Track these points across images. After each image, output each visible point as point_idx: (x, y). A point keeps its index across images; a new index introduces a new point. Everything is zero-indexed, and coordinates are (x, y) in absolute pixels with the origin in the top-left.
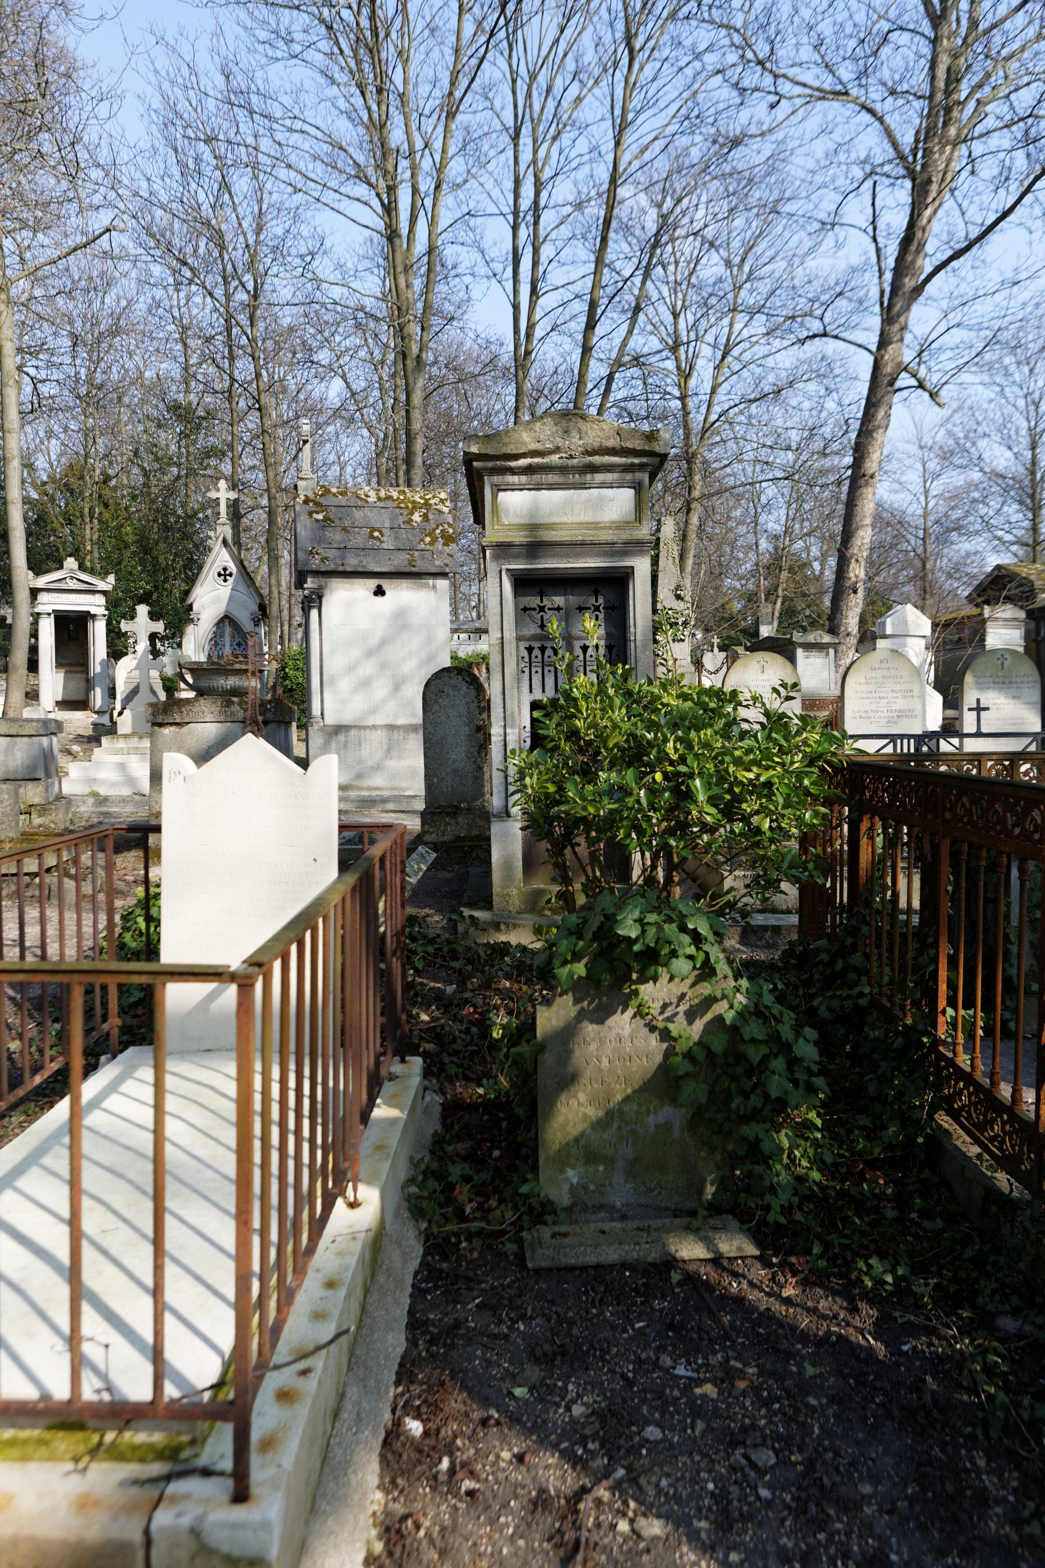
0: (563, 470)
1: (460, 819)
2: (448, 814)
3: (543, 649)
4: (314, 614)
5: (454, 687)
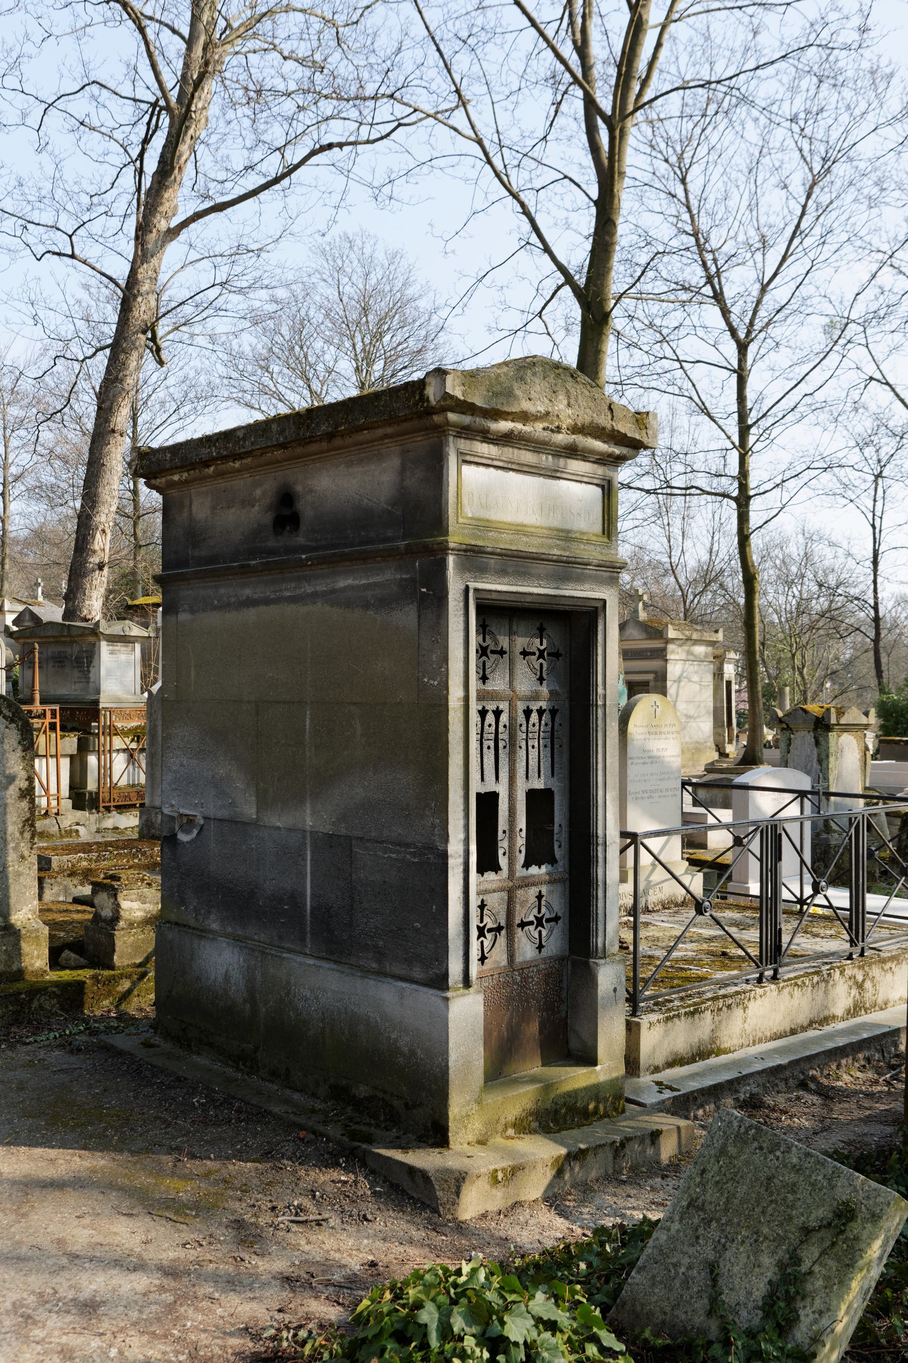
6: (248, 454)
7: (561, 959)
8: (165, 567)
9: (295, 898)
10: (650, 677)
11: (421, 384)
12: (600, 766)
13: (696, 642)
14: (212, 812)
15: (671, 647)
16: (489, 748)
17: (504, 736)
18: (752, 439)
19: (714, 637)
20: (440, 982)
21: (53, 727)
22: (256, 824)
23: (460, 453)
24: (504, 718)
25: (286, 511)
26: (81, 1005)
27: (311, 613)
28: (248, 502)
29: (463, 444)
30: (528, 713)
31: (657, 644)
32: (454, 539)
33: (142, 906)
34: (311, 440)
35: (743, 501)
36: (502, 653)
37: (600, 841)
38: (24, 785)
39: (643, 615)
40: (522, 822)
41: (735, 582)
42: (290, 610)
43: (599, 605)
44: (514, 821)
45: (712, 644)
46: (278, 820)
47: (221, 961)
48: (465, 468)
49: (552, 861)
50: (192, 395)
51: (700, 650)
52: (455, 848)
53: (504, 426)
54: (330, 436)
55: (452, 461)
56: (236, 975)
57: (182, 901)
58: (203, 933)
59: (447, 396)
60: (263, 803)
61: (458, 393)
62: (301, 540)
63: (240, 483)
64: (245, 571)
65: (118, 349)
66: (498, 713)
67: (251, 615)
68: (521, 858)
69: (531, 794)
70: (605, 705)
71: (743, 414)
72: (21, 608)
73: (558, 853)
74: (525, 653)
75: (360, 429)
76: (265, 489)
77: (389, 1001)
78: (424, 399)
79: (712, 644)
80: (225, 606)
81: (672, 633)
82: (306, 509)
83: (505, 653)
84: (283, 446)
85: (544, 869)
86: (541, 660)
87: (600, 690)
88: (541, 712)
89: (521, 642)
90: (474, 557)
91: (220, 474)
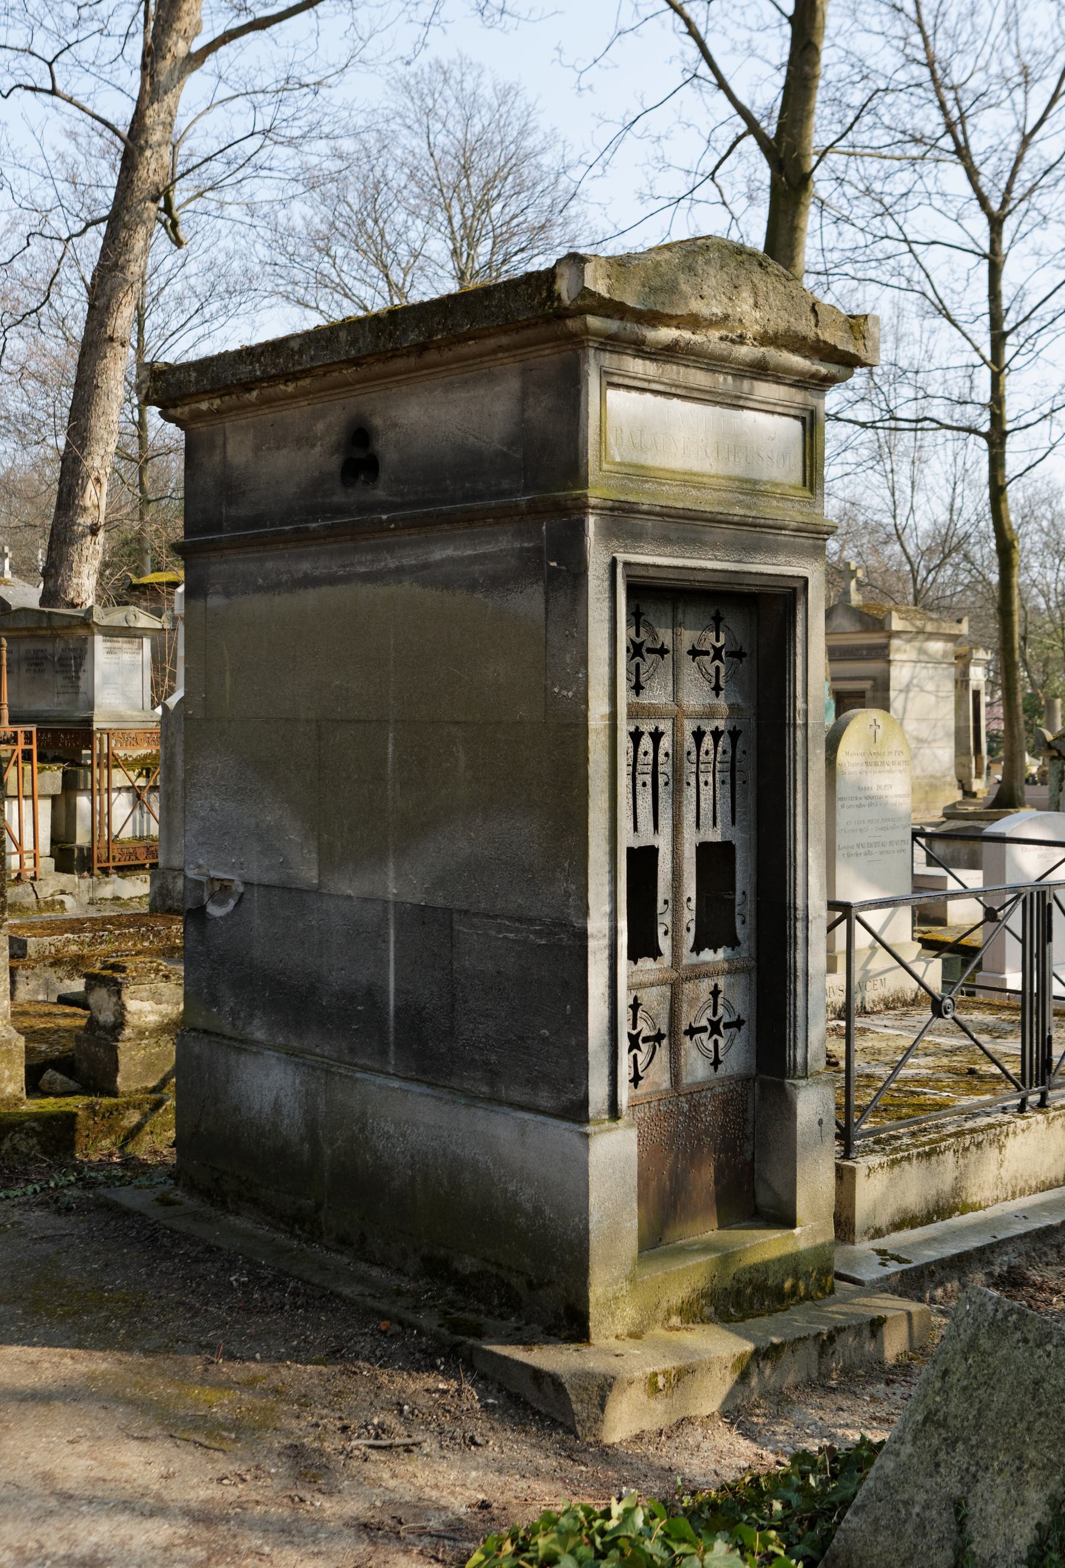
6: (306, 373)
7: (745, 1080)
9: (373, 996)
10: (867, 685)
11: (549, 276)
12: (800, 810)
15: (895, 643)
16: (706, 783)
17: (665, 767)
18: (1008, 352)
20: (577, 1111)
21: (27, 756)
22: (317, 892)
23: (604, 373)
24: (666, 744)
25: (359, 453)
26: (71, 1146)
28: (306, 441)
29: (609, 360)
30: (698, 735)
31: (876, 639)
32: (595, 495)
34: (395, 354)
36: (662, 651)
37: (800, 914)
40: (690, 889)
41: (986, 551)
42: (365, 591)
43: (798, 584)
44: (679, 885)
45: (954, 638)
46: (348, 886)
47: (269, 1085)
48: (612, 394)
49: (733, 942)
50: (221, 288)
51: (937, 647)
52: (597, 924)
53: (666, 334)
54: (422, 348)
57: (215, 1000)
58: (242, 1044)
59: (585, 293)
60: (328, 862)
62: (380, 494)
63: (295, 415)
64: (302, 537)
65: (119, 223)
66: (656, 736)
67: (310, 598)
68: (689, 939)
69: (704, 850)
70: (806, 725)
71: (996, 317)
74: (694, 653)
75: (464, 338)
77: (503, 1138)
78: (553, 296)
79: (954, 638)
80: (274, 587)
81: (897, 624)
82: (388, 451)
83: (667, 651)
84: (355, 362)
85: (721, 954)
86: (717, 662)
87: (800, 704)
88: (716, 734)
89: (688, 637)
90: (622, 517)
91: (266, 402)
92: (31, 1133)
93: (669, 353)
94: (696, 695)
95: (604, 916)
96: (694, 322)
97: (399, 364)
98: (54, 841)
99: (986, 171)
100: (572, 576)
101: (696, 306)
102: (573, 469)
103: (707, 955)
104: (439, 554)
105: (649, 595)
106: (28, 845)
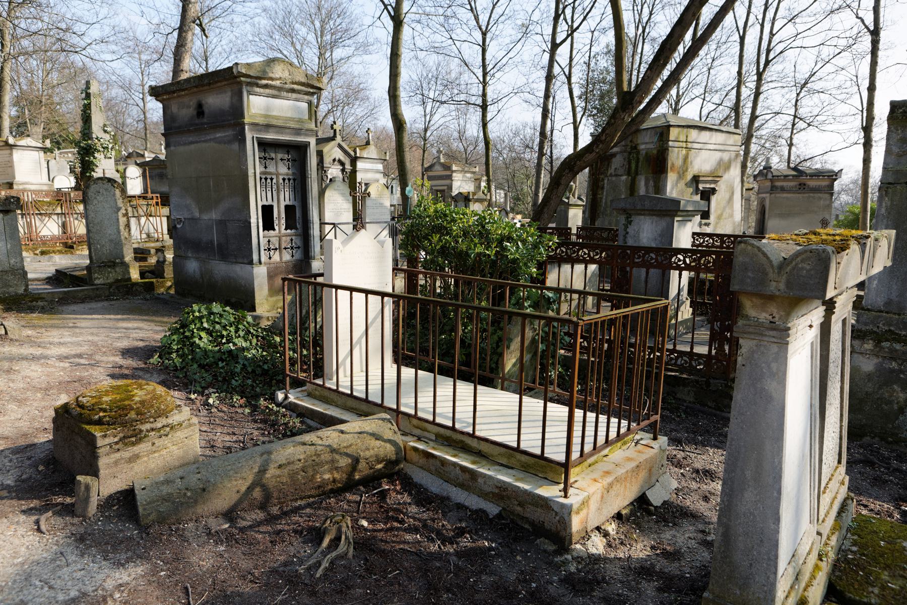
0: (280, 89)
1: (117, 269)
2: (109, 267)
3: (266, 179)
4: (701, 179)
5: (106, 190)
6: (186, 89)
7: (301, 261)
8: (165, 129)
9: (212, 242)
10: (445, 188)
11: (230, 68)
13: (466, 172)
14: (186, 217)
15: (454, 174)
17: (275, 187)
18: (488, 78)
19: (474, 170)
20: (251, 263)
21: (157, 204)
22: (199, 219)
23: (248, 91)
24: (274, 181)
25: (200, 110)
26: (153, 290)
27: (208, 146)
28: (189, 107)
29: (249, 88)
30: (284, 180)
31: (448, 173)
32: (246, 120)
33: (399, 439)
34: (203, 86)
35: (484, 107)
36: (272, 159)
38: (124, 212)
39: (442, 161)
40: (283, 215)
41: (482, 145)
42: (204, 145)
44: (279, 215)
45: (474, 173)
46: (205, 217)
47: (192, 266)
48: (251, 97)
49: (296, 229)
50: (234, 50)
51: (469, 175)
52: (253, 220)
53: (264, 82)
54: (210, 84)
55: (245, 94)
56: (197, 270)
57: (180, 248)
58: (186, 258)
59: (239, 72)
60: (201, 212)
61: (244, 71)
62: (205, 120)
63: (186, 100)
64: (189, 131)
65: (182, 30)
66: (272, 179)
67: (193, 147)
68: (284, 227)
69: (287, 207)
71: (484, 66)
72: (153, 156)
73: (298, 226)
74: (282, 160)
75: (216, 82)
76: (193, 102)
77: (238, 270)
78: (233, 73)
79: (474, 173)
80: (185, 144)
81: (454, 168)
82: (206, 111)
84: (196, 87)
85: (293, 231)
88: (289, 180)
89: (280, 156)
90: (254, 125)
91: (179, 96)
92: (141, 286)
93: (266, 86)
94: (283, 169)
95: (255, 218)
96: (272, 79)
97: (205, 88)
98: (168, 230)
99: (481, 18)
100: (243, 141)
101: (271, 75)
102: (242, 115)
103: (289, 231)
104: (218, 135)
105: (264, 145)
106: (160, 230)
